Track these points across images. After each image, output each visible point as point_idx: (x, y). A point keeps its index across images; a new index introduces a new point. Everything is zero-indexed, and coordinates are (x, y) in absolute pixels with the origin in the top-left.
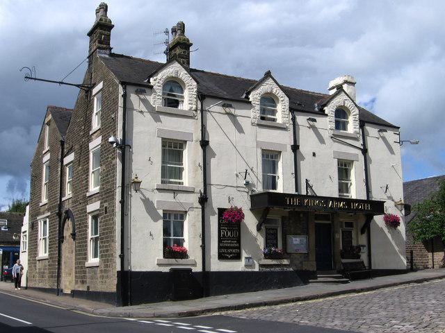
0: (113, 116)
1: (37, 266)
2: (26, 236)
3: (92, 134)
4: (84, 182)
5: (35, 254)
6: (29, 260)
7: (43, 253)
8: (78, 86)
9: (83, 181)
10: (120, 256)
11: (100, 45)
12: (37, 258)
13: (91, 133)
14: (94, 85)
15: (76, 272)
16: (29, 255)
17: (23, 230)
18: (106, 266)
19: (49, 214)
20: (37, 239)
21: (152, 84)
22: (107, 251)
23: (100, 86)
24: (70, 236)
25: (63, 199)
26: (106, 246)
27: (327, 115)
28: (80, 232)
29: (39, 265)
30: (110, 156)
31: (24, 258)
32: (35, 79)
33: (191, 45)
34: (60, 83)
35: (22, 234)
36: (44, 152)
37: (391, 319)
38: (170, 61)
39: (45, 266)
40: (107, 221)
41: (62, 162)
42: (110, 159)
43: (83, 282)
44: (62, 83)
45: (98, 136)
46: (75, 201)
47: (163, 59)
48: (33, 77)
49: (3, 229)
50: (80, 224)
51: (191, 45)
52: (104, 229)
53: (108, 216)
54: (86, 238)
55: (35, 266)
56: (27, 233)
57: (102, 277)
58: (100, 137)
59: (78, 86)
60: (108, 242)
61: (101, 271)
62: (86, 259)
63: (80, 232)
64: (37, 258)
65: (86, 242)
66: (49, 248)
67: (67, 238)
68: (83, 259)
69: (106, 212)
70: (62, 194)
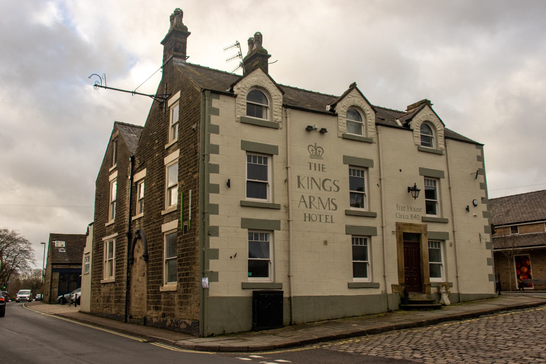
0: (194, 127)
1: (102, 289)
2: (89, 257)
3: (168, 148)
4: (159, 199)
5: (100, 277)
6: (92, 284)
7: (108, 277)
8: (151, 96)
9: (156, 198)
10: (69, 265)
11: (175, 53)
12: (102, 281)
13: (166, 146)
14: (171, 96)
15: (148, 297)
16: (92, 278)
17: (85, 252)
18: (186, 291)
19: (116, 234)
20: (101, 261)
21: (235, 93)
22: (187, 274)
23: (178, 95)
24: (141, 258)
25: (133, 218)
26: (186, 269)
27: (412, 130)
28: (153, 253)
29: (104, 289)
30: (190, 170)
31: (86, 280)
32: (106, 88)
33: (270, 56)
34: (132, 92)
35: (84, 256)
36: (110, 170)
37: (489, 350)
38: (247, 73)
39: (111, 290)
40: (186, 241)
41: (132, 179)
42: (190, 174)
43: (157, 308)
44: (135, 93)
45: (175, 150)
46: (147, 220)
47: (240, 72)
48: (104, 85)
49: (60, 251)
50: (153, 245)
51: (270, 56)
52: (183, 251)
53: (188, 236)
54: (161, 260)
55: (99, 290)
56: (91, 255)
57: (181, 303)
58: (178, 151)
59: (151, 96)
60: (188, 264)
61: (180, 297)
62: (161, 283)
63: (153, 253)
64: (102, 281)
65: (161, 264)
66: (116, 271)
67: (138, 259)
68: (157, 282)
69: (186, 232)
70: (132, 212)
